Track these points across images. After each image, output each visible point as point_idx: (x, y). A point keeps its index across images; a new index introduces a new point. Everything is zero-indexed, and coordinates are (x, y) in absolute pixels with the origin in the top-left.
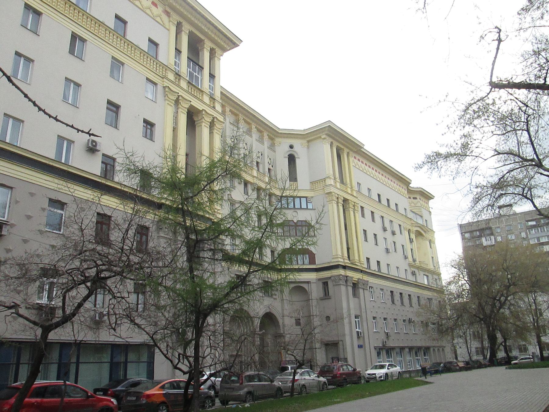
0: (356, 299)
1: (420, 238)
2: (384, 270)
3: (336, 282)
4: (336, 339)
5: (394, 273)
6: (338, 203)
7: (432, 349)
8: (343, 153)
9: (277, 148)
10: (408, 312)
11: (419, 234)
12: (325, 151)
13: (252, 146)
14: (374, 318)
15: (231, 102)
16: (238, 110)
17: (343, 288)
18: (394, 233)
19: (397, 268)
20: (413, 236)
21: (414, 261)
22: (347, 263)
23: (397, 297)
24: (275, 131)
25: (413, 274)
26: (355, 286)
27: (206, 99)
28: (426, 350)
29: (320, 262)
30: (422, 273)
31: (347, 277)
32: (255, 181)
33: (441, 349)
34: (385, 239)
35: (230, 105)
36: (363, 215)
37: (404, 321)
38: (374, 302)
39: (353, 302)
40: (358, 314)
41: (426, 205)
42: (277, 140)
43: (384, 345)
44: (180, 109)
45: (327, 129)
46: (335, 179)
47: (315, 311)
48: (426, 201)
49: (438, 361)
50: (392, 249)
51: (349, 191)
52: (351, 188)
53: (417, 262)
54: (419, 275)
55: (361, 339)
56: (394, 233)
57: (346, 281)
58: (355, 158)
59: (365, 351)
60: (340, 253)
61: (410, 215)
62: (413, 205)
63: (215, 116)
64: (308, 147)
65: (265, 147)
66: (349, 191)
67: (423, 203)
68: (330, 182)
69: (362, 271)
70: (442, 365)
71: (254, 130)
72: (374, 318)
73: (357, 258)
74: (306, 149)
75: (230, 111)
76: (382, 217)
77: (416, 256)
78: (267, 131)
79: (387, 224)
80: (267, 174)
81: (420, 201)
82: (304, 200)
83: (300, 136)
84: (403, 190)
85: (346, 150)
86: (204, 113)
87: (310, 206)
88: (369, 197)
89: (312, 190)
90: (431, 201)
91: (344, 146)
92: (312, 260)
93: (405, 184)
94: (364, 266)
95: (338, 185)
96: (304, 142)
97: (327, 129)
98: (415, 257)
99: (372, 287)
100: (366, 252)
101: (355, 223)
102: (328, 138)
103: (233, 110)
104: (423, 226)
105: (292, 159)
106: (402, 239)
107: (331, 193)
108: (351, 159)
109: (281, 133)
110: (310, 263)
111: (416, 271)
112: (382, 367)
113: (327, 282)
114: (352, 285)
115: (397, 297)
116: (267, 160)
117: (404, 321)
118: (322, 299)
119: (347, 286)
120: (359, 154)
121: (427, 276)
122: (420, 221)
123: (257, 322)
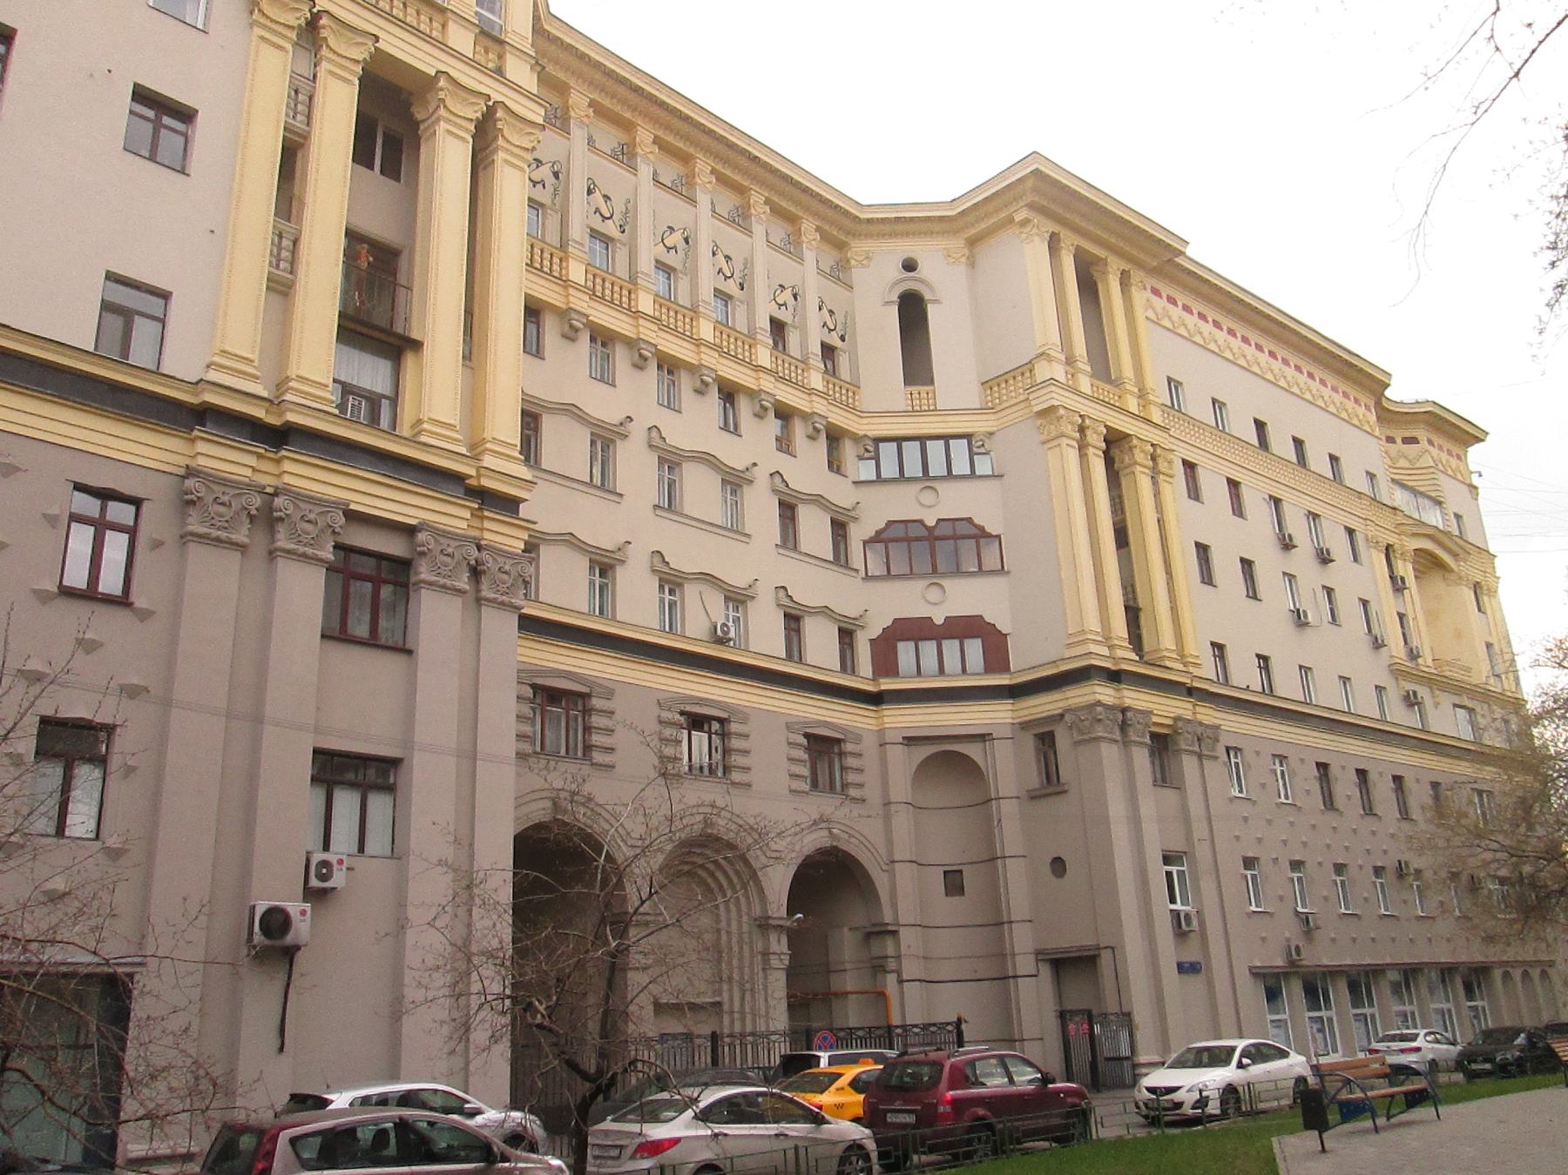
0: (1169, 795)
1: (1437, 584)
2: (1288, 687)
3: (1081, 732)
4: (1088, 941)
5: (1327, 697)
6: (1082, 447)
7: (1497, 974)
8: (1105, 273)
9: (858, 275)
10: (1385, 838)
11: (1429, 564)
12: (1031, 270)
13: (748, 264)
14: (1249, 863)
15: (654, 110)
16: (686, 138)
17: (1109, 753)
18: (1324, 558)
19: (1345, 680)
20: (1405, 569)
21: (1413, 655)
22: (1125, 657)
23: (1345, 787)
24: (846, 213)
25: (1411, 701)
26: (1162, 744)
27: (462, 39)
28: (1474, 978)
29: (1025, 661)
30: (1447, 700)
31: (1124, 710)
32: (819, 406)
33: (1535, 973)
34: (1291, 577)
35: (655, 121)
36: (1194, 493)
37: (1378, 871)
38: (1244, 804)
39: (1151, 801)
40: (1177, 845)
41: (1454, 462)
42: (859, 247)
43: (1292, 963)
44: (324, 65)
45: (1030, 183)
46: (1070, 361)
47: (1011, 836)
48: (1455, 450)
49: (1508, 1023)
50: (1317, 612)
51: (1132, 405)
52: (1142, 395)
53: (1426, 660)
54: (1436, 705)
55: (1194, 940)
56: (1324, 558)
57: (1124, 726)
58: (1156, 292)
59: (1210, 984)
60: (1093, 623)
61: (1400, 498)
62: (1403, 463)
63: (496, 97)
64: (972, 263)
65: (809, 272)
66: (1132, 405)
67: (1444, 456)
68: (1043, 371)
69: (1190, 692)
70: (1521, 1040)
71: (759, 208)
72: (1249, 863)
73: (1167, 641)
74: (962, 269)
75: (656, 141)
76: (1277, 502)
77: (1423, 639)
78: (816, 214)
79: (1296, 526)
80: (816, 362)
81: (1430, 452)
82: (959, 448)
83: (936, 227)
84: (1361, 411)
85: (1115, 265)
86: (442, 83)
87: (983, 466)
88: (1220, 428)
89: (985, 409)
90: (1475, 453)
91: (1108, 250)
92: (996, 656)
93: (1372, 392)
94: (1196, 672)
95: (1085, 384)
96: (957, 244)
98: (1414, 643)
99: (1237, 750)
100: (1203, 624)
101: (1160, 522)
103: (607, 102)
104: (1448, 534)
106: (1362, 578)
107: (1052, 409)
108: (1140, 297)
109: (869, 221)
110: (989, 668)
111: (1423, 692)
112: (1219, 1057)
113: (1051, 735)
114: (1147, 740)
115: (1345, 787)
116: (814, 319)
117: (1378, 871)
118: (1034, 796)
119: (1126, 743)
120: (1173, 280)
121: (1471, 711)
122: (1433, 517)
123: (778, 882)
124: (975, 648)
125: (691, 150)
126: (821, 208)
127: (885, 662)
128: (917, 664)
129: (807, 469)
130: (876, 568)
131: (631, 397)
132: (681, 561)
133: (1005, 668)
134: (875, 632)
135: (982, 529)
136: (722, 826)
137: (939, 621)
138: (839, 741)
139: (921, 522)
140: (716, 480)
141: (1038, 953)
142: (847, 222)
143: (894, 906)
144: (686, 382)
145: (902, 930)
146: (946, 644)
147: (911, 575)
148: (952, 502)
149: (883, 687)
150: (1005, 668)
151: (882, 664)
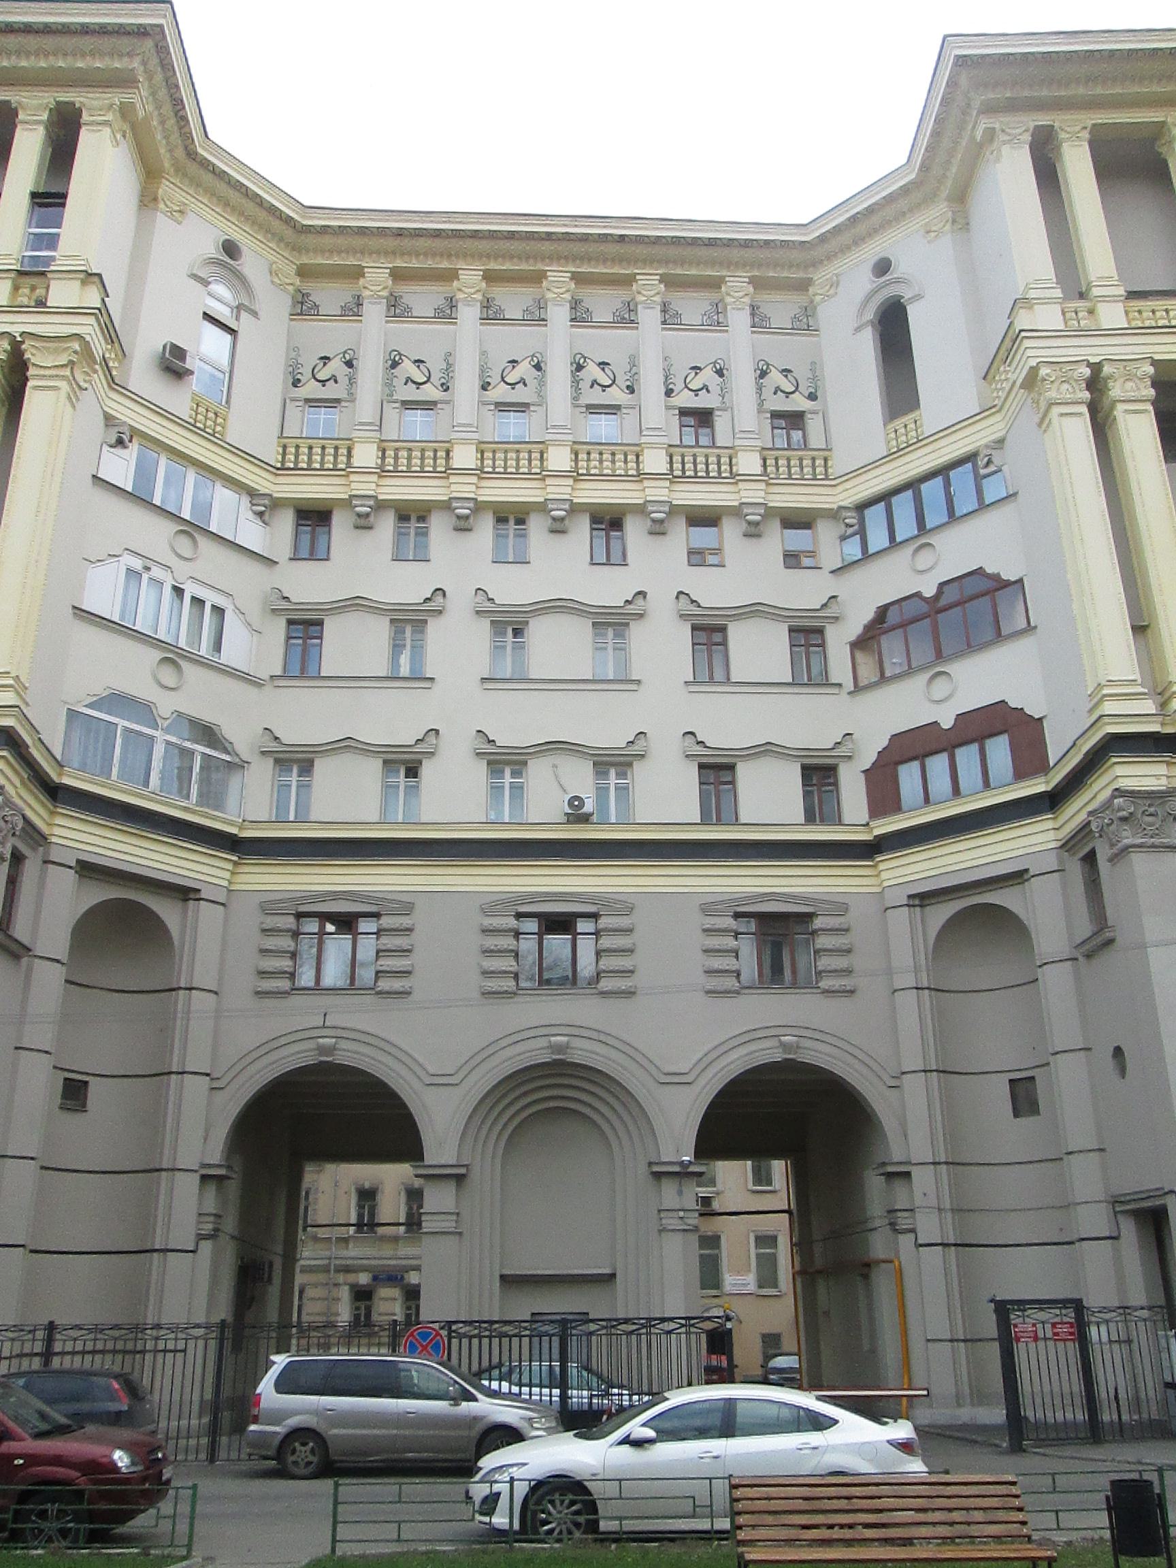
45: (964, 80)
83: (903, 204)
89: (987, 410)
97: (964, 80)
102: (996, 122)
105: (892, 328)
110: (1021, 773)
124: (1000, 750)
125: (540, 266)
126: (748, 254)
127: (884, 797)
128: (927, 793)
129: (747, 573)
130: (868, 672)
131: (462, 565)
132: (294, 734)
133: (1042, 767)
134: (868, 758)
135: (996, 578)
136: (583, 1052)
137: (947, 724)
138: (810, 916)
139: (918, 595)
140: (582, 629)
141: (1115, 1201)
142: (795, 255)
143: (175, 1149)
144: (634, 530)
145: (915, 1172)
146: (961, 753)
147: (910, 671)
148: (958, 552)
149: (877, 832)
150: (1042, 767)
151: (864, 804)
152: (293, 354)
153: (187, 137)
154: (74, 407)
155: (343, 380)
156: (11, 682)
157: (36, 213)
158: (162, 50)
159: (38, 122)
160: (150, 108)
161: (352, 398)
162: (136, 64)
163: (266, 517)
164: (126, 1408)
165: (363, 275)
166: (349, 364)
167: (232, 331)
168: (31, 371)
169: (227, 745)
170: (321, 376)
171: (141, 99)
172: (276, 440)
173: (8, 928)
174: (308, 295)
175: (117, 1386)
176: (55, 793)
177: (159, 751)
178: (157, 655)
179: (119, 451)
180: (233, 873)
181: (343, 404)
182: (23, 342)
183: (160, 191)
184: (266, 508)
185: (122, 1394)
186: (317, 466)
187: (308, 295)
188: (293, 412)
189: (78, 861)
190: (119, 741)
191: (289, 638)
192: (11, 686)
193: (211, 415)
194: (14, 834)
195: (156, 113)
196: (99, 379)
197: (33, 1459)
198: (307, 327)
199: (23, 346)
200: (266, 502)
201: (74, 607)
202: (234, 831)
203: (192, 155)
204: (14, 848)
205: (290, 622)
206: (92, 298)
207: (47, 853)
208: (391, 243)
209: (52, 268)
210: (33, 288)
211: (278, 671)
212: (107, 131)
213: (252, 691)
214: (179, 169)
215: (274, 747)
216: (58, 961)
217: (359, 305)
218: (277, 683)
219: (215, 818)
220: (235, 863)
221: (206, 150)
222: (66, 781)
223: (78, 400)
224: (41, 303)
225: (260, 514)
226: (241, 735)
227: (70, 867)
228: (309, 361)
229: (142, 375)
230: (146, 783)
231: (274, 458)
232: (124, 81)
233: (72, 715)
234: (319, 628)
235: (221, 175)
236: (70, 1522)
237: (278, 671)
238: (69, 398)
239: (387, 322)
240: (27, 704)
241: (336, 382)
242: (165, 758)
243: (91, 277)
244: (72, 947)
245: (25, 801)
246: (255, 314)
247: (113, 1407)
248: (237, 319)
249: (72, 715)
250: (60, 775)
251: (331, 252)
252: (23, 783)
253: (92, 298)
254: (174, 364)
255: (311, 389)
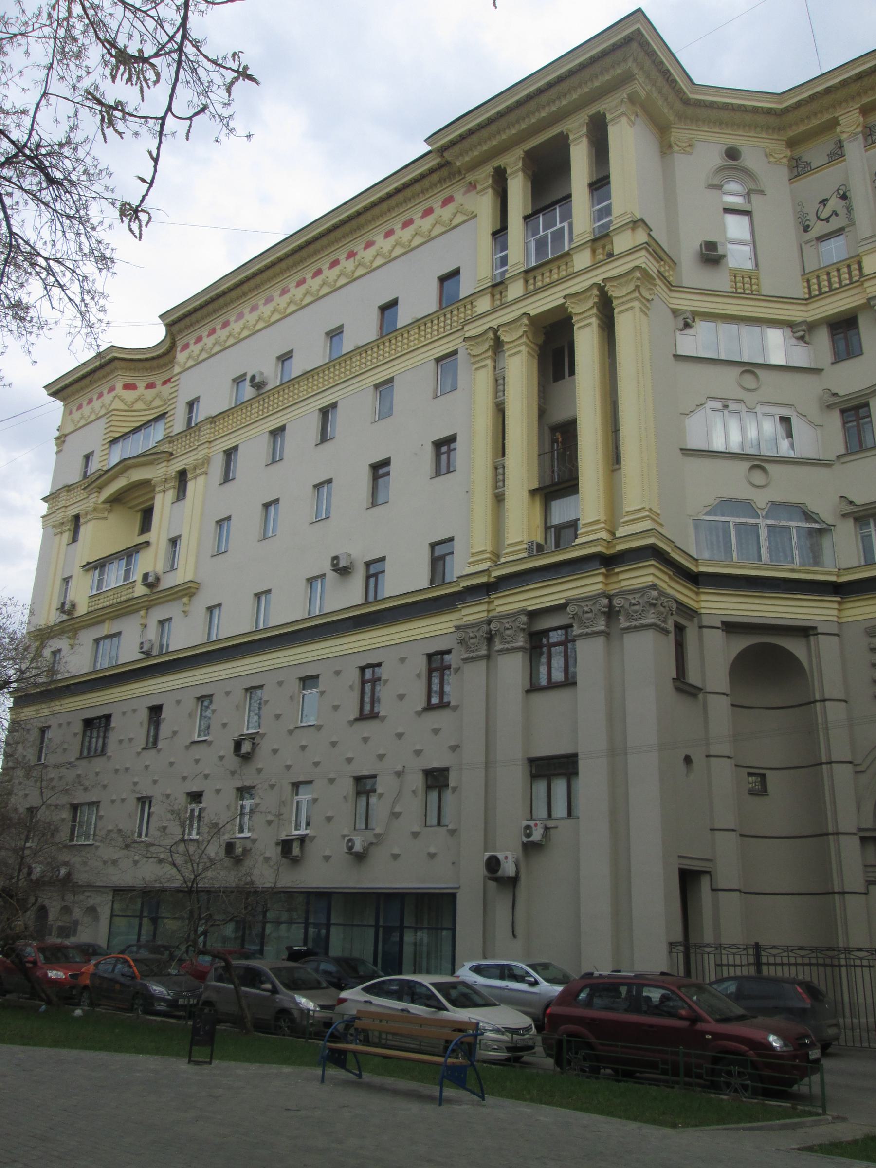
152: (799, 208)
153: (679, 92)
154: (646, 314)
155: (842, 212)
156: (647, 513)
157: (595, 197)
158: (645, 45)
159: (581, 137)
160: (648, 88)
161: (852, 222)
162: (630, 63)
163: (807, 338)
164: (809, 1006)
165: (838, 124)
166: (844, 197)
167: (747, 213)
168: (615, 303)
169: (814, 516)
170: (823, 216)
171: (641, 87)
172: (800, 278)
173: (684, 679)
174: (800, 158)
175: (800, 991)
176: (695, 579)
177: (763, 533)
178: (747, 465)
179: (688, 331)
180: (839, 610)
181: (847, 230)
182: (605, 286)
183: (672, 139)
184: (802, 332)
185: (804, 996)
186: (837, 285)
187: (800, 158)
188: (808, 250)
189: (723, 623)
190: (733, 533)
191: (844, 423)
192: (648, 516)
193: (746, 280)
194: (672, 614)
195: (654, 89)
196: (660, 288)
197: (717, 1036)
198: (803, 183)
199: (606, 288)
200: (804, 327)
201: (681, 449)
202: (833, 578)
203: (687, 102)
204: (675, 622)
205: (843, 411)
206: (641, 237)
207: (700, 620)
208: (855, 87)
209: (612, 228)
210: (604, 247)
211: (843, 451)
212: (624, 119)
213: (824, 471)
214: (681, 117)
215: (850, 509)
216: (723, 694)
217: (841, 147)
218: (843, 460)
219: (815, 573)
220: (839, 603)
221: (697, 93)
222: (702, 569)
223: (648, 309)
224: (610, 255)
225: (802, 338)
226: (825, 508)
227: (718, 628)
228: (811, 208)
229: (690, 272)
230: (760, 559)
231: (801, 291)
232: (627, 78)
233: (697, 523)
234: (866, 409)
235: (712, 105)
236: (746, 1080)
237: (843, 451)
238: (642, 310)
239: (866, 151)
240: (661, 525)
241: (837, 215)
242: (769, 536)
243: (637, 223)
244: (731, 682)
245: (676, 590)
246: (761, 192)
247: (801, 1005)
248: (750, 202)
249: (697, 523)
250: (697, 566)
251: (808, 117)
252: (670, 577)
253: (641, 237)
254: (711, 255)
255: (819, 228)
